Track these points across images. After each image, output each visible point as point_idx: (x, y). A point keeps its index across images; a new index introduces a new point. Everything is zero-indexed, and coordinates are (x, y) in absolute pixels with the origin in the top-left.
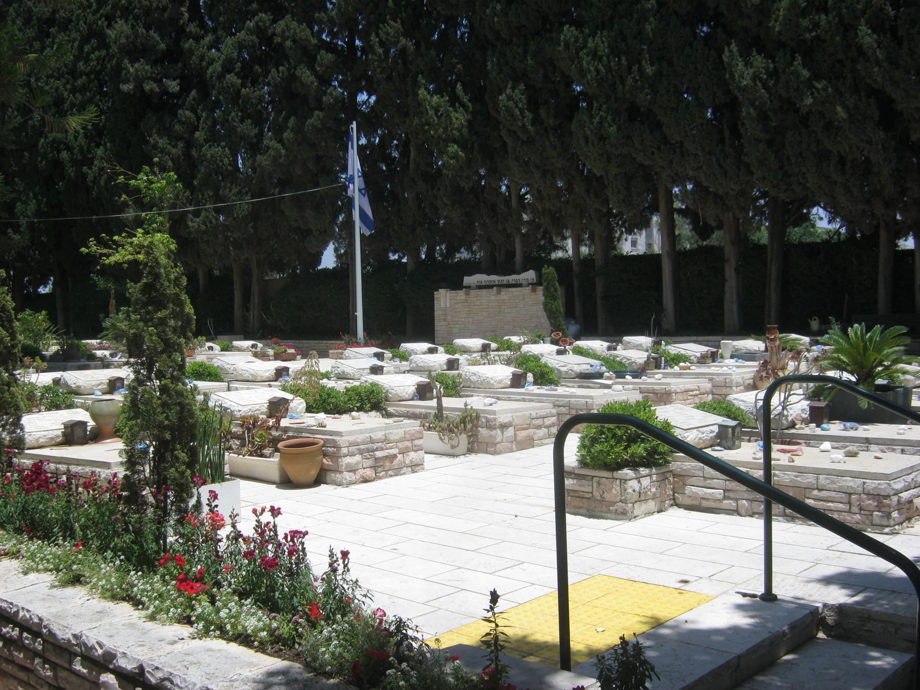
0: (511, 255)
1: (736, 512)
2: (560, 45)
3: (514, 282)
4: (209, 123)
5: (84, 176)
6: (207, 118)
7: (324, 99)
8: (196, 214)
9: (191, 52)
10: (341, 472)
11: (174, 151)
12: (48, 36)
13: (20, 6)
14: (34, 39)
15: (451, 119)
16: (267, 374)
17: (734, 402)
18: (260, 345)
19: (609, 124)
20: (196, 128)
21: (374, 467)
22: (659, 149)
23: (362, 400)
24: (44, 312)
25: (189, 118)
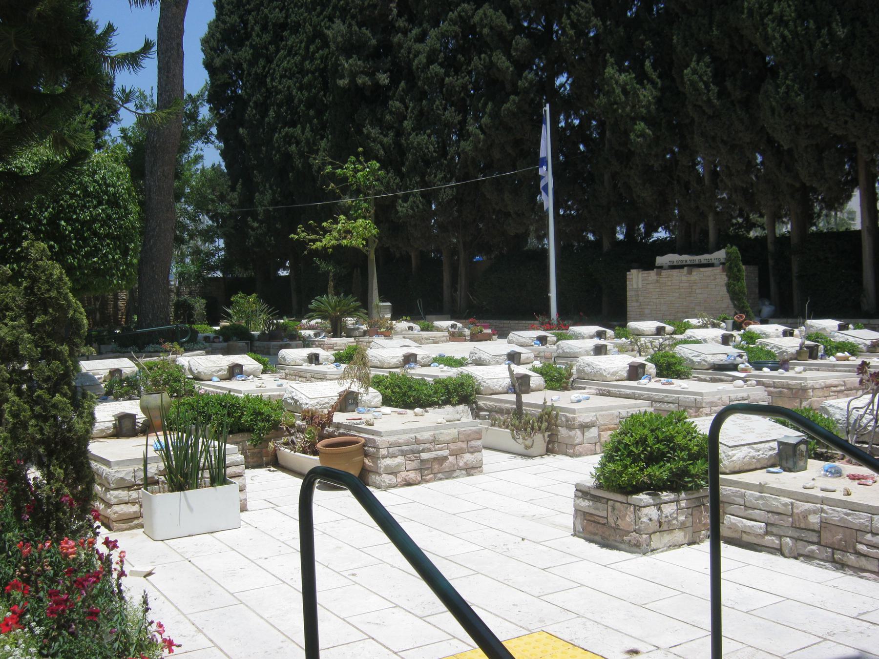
0: (705, 233)
1: (779, 551)
2: (743, 13)
3: (705, 262)
4: (416, 112)
5: (310, 166)
6: (414, 108)
7: (520, 83)
8: (405, 198)
9: (400, 46)
10: (380, 474)
11: (385, 140)
12: (282, 40)
13: (258, 14)
14: (270, 43)
15: (638, 96)
16: (395, 361)
17: (830, 409)
18: (459, 325)
19: (796, 93)
20: (405, 118)
21: (420, 470)
22: (853, 117)
23: (449, 392)
24: (254, 295)
25: (399, 108)
